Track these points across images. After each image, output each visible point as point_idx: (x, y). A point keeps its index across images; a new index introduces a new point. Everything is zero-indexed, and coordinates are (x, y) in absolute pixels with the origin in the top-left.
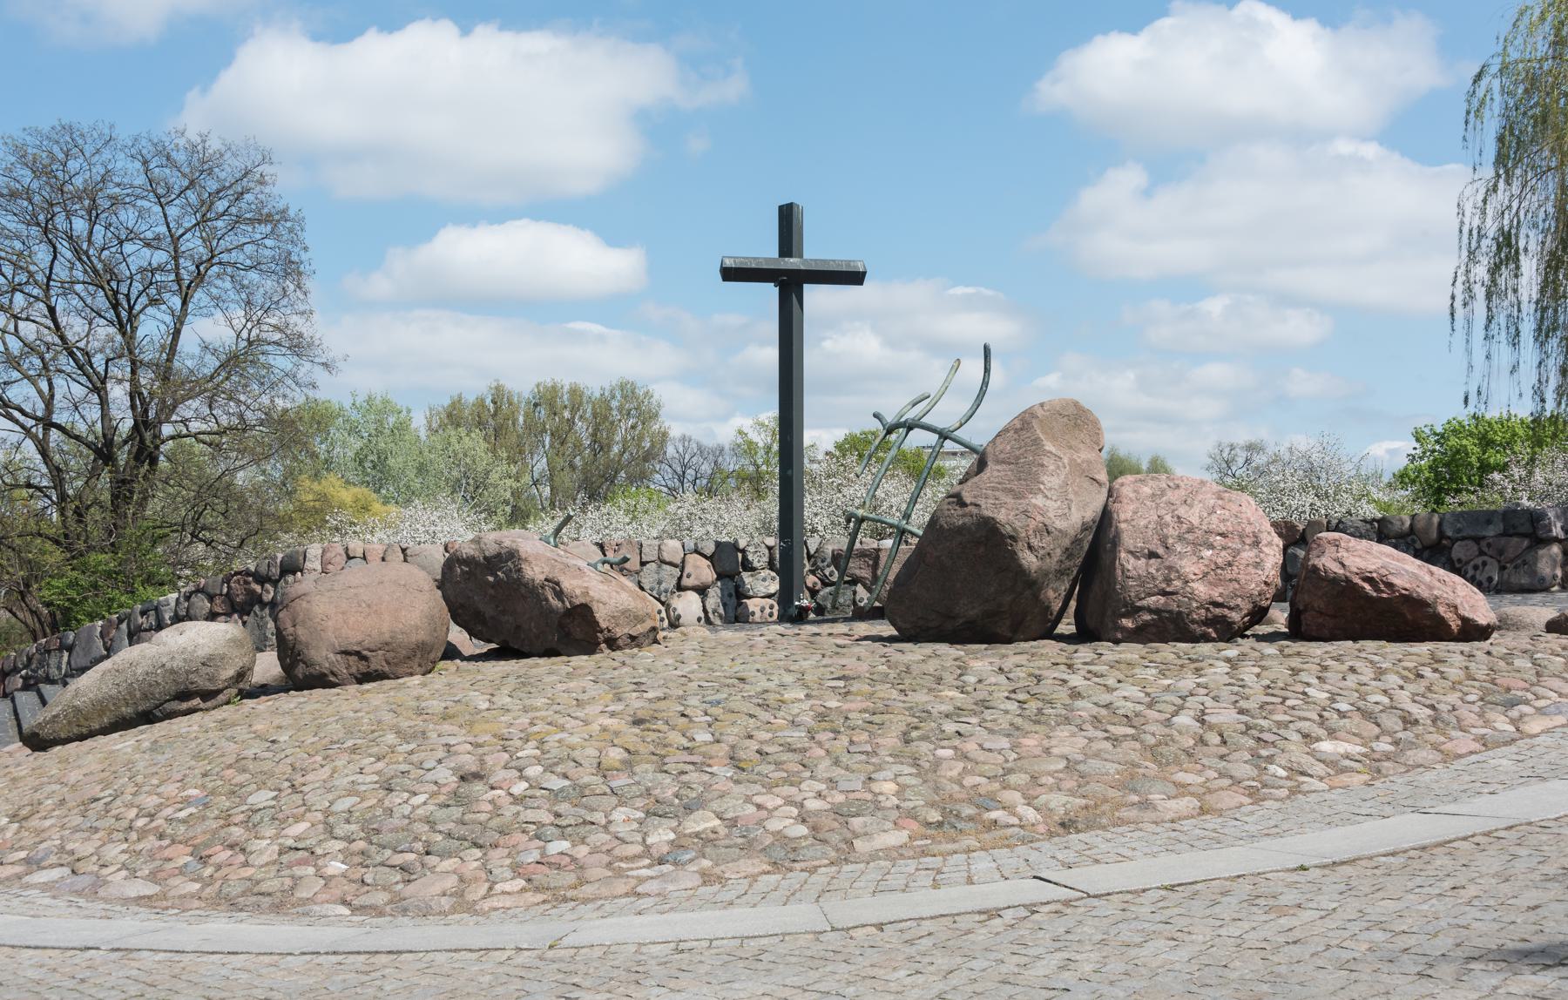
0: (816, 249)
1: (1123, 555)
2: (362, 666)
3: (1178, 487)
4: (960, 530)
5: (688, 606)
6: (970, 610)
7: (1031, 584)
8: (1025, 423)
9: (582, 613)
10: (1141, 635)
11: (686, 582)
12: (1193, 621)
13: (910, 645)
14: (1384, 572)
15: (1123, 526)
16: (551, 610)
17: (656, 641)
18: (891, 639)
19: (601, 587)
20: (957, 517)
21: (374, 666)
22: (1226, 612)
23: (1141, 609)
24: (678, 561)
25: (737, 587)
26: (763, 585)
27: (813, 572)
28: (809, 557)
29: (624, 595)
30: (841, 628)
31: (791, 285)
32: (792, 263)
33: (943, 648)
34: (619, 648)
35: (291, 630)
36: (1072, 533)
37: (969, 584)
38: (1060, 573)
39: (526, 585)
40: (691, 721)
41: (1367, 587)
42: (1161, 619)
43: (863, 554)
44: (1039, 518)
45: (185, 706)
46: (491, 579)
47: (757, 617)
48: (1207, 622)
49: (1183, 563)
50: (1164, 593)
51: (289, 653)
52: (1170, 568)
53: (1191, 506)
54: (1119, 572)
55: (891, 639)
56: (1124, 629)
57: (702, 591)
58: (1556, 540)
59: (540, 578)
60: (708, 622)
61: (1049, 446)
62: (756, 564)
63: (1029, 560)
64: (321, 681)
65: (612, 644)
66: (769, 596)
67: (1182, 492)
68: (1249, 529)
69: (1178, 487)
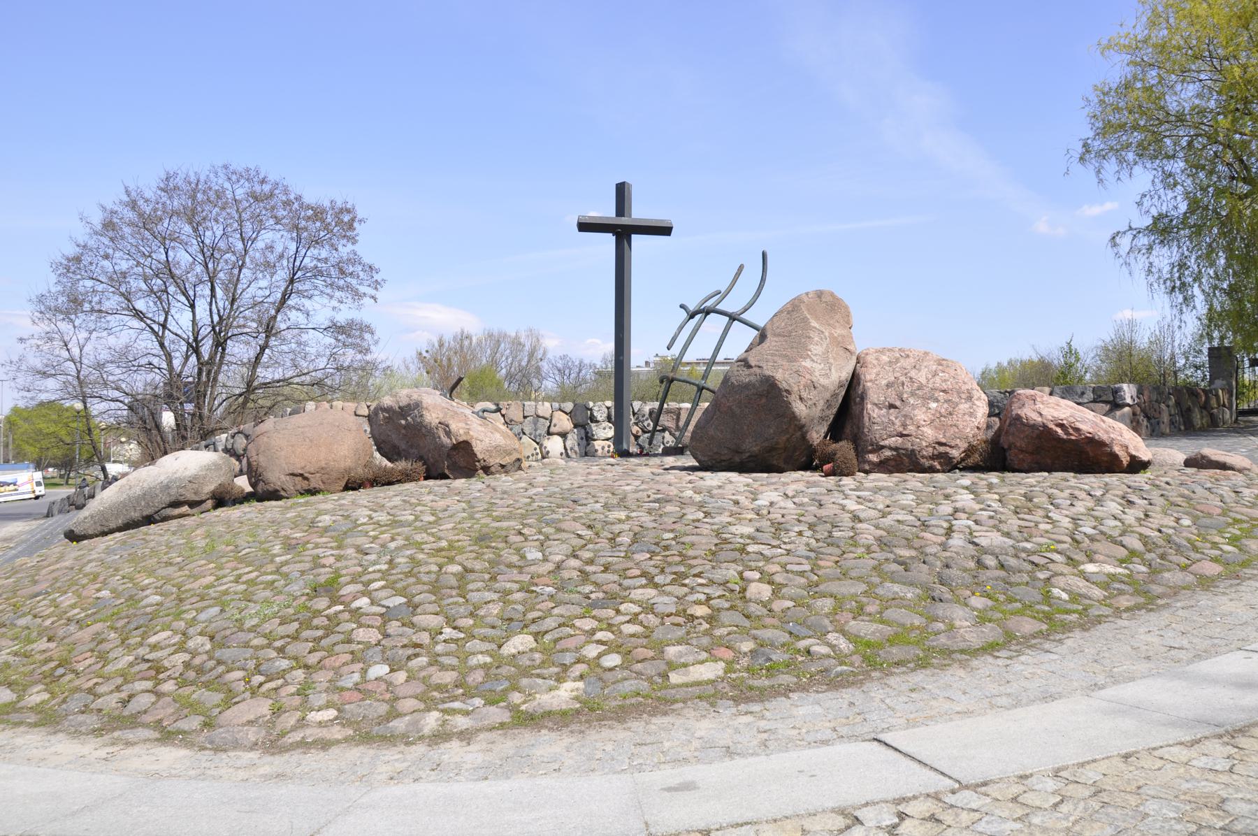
0: (640, 212)
1: (869, 406)
2: (305, 485)
3: (908, 356)
4: (746, 386)
5: (554, 445)
6: (751, 446)
7: (800, 428)
8: (793, 308)
9: (464, 447)
10: (886, 467)
11: (553, 429)
12: (923, 457)
13: (708, 474)
14: (1072, 419)
15: (869, 384)
16: (443, 446)
17: (520, 468)
18: (693, 469)
19: (480, 428)
20: (744, 376)
21: (312, 485)
22: (948, 449)
23: (883, 447)
24: (548, 416)
25: (587, 433)
26: (604, 431)
27: (636, 424)
28: (634, 414)
29: (498, 435)
30: (657, 460)
31: (623, 233)
32: (624, 221)
33: (733, 476)
34: (492, 473)
35: (255, 458)
36: (832, 388)
37: (751, 428)
38: (822, 419)
39: (425, 427)
40: (526, 540)
41: (1059, 430)
42: (898, 455)
43: (669, 412)
44: (808, 376)
45: (177, 511)
46: (403, 422)
47: (600, 452)
48: (933, 457)
49: (916, 412)
50: (902, 435)
51: (254, 474)
52: (905, 416)
53: (919, 370)
54: (866, 419)
55: (693, 469)
56: (870, 462)
57: (564, 435)
58: (1128, 405)
59: (435, 422)
60: (568, 456)
61: (814, 323)
62: (599, 418)
63: (800, 409)
64: (274, 495)
65: (487, 470)
66: (608, 439)
67: (912, 360)
68: (964, 388)
69: (908, 356)
